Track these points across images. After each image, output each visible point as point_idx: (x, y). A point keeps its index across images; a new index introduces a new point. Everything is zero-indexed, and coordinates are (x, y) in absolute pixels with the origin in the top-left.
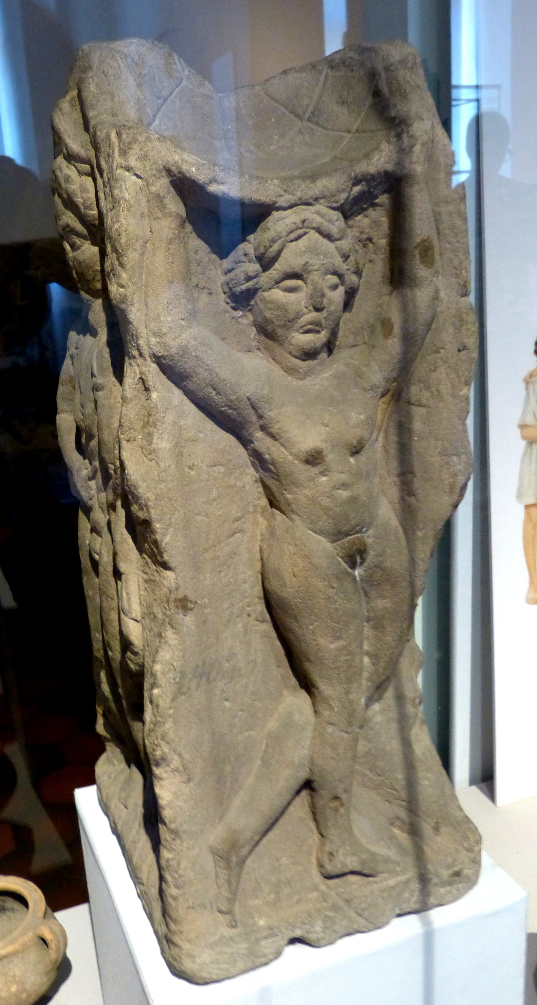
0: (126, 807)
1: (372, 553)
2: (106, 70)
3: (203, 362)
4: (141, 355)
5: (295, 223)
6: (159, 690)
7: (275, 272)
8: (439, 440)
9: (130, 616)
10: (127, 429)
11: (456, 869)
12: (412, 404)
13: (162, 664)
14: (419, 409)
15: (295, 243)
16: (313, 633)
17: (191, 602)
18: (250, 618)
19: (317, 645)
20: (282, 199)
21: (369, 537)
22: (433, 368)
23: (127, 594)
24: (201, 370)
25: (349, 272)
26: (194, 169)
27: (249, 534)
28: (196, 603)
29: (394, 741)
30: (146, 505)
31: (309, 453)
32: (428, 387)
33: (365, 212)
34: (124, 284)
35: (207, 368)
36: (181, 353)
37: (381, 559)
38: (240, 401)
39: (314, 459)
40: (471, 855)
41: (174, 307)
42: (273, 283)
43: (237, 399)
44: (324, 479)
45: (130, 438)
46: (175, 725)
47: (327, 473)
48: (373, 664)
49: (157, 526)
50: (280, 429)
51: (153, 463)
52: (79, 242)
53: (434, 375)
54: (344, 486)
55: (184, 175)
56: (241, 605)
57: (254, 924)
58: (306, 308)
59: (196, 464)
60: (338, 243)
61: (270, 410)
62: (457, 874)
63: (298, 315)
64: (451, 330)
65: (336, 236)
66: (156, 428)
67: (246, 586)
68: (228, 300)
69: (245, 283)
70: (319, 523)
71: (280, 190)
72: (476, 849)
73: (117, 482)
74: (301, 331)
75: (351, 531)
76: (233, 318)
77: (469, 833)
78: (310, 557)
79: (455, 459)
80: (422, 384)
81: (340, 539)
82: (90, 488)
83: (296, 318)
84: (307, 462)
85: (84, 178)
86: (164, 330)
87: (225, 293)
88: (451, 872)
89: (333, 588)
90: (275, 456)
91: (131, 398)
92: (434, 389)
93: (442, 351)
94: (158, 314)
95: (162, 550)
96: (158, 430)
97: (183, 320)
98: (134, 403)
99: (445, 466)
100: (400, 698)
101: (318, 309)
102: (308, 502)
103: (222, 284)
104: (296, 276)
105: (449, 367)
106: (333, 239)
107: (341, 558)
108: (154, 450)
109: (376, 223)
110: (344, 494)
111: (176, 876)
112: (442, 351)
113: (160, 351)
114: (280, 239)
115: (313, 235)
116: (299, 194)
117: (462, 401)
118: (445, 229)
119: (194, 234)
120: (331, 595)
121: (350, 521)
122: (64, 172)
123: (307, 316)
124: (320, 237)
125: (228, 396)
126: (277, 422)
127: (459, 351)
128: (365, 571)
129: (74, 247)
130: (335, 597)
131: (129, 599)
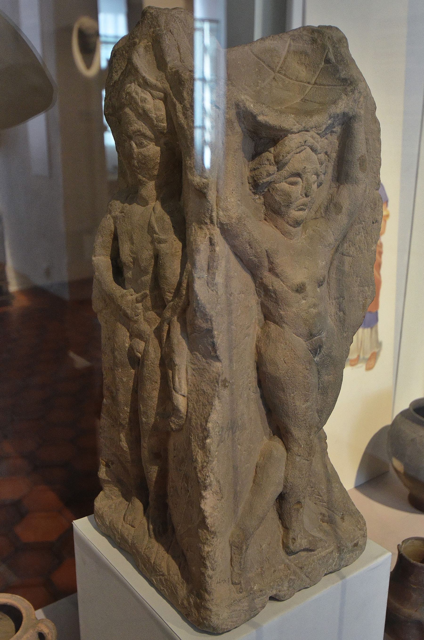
0: (133, 526)
2: (172, 30)
4: (212, 222)
5: (300, 142)
6: (210, 439)
7: (285, 172)
9: (180, 393)
11: (355, 542)
14: (348, 257)
15: (298, 155)
16: (293, 398)
18: (249, 391)
20: (296, 127)
23: (179, 378)
26: (252, 105)
30: (210, 320)
34: (207, 176)
39: (300, 289)
40: (361, 532)
44: (304, 301)
46: (218, 462)
49: (216, 333)
50: (282, 270)
52: (146, 143)
53: (358, 237)
54: (315, 306)
55: (246, 109)
57: (252, 589)
58: (301, 195)
62: (356, 545)
64: (369, 210)
68: (251, 188)
71: (294, 121)
72: (365, 528)
73: (180, 304)
77: (360, 520)
82: (137, 308)
84: (297, 291)
85: (157, 101)
86: (230, 207)
87: (249, 183)
88: (353, 544)
89: (307, 369)
90: (276, 287)
94: (226, 197)
95: (217, 349)
101: (307, 196)
103: (248, 177)
104: (298, 175)
105: (367, 233)
108: (216, 284)
110: (313, 311)
111: (213, 562)
113: (225, 220)
116: (304, 125)
122: (140, 95)
127: (373, 223)
129: (140, 145)
130: (308, 375)
131: (180, 382)
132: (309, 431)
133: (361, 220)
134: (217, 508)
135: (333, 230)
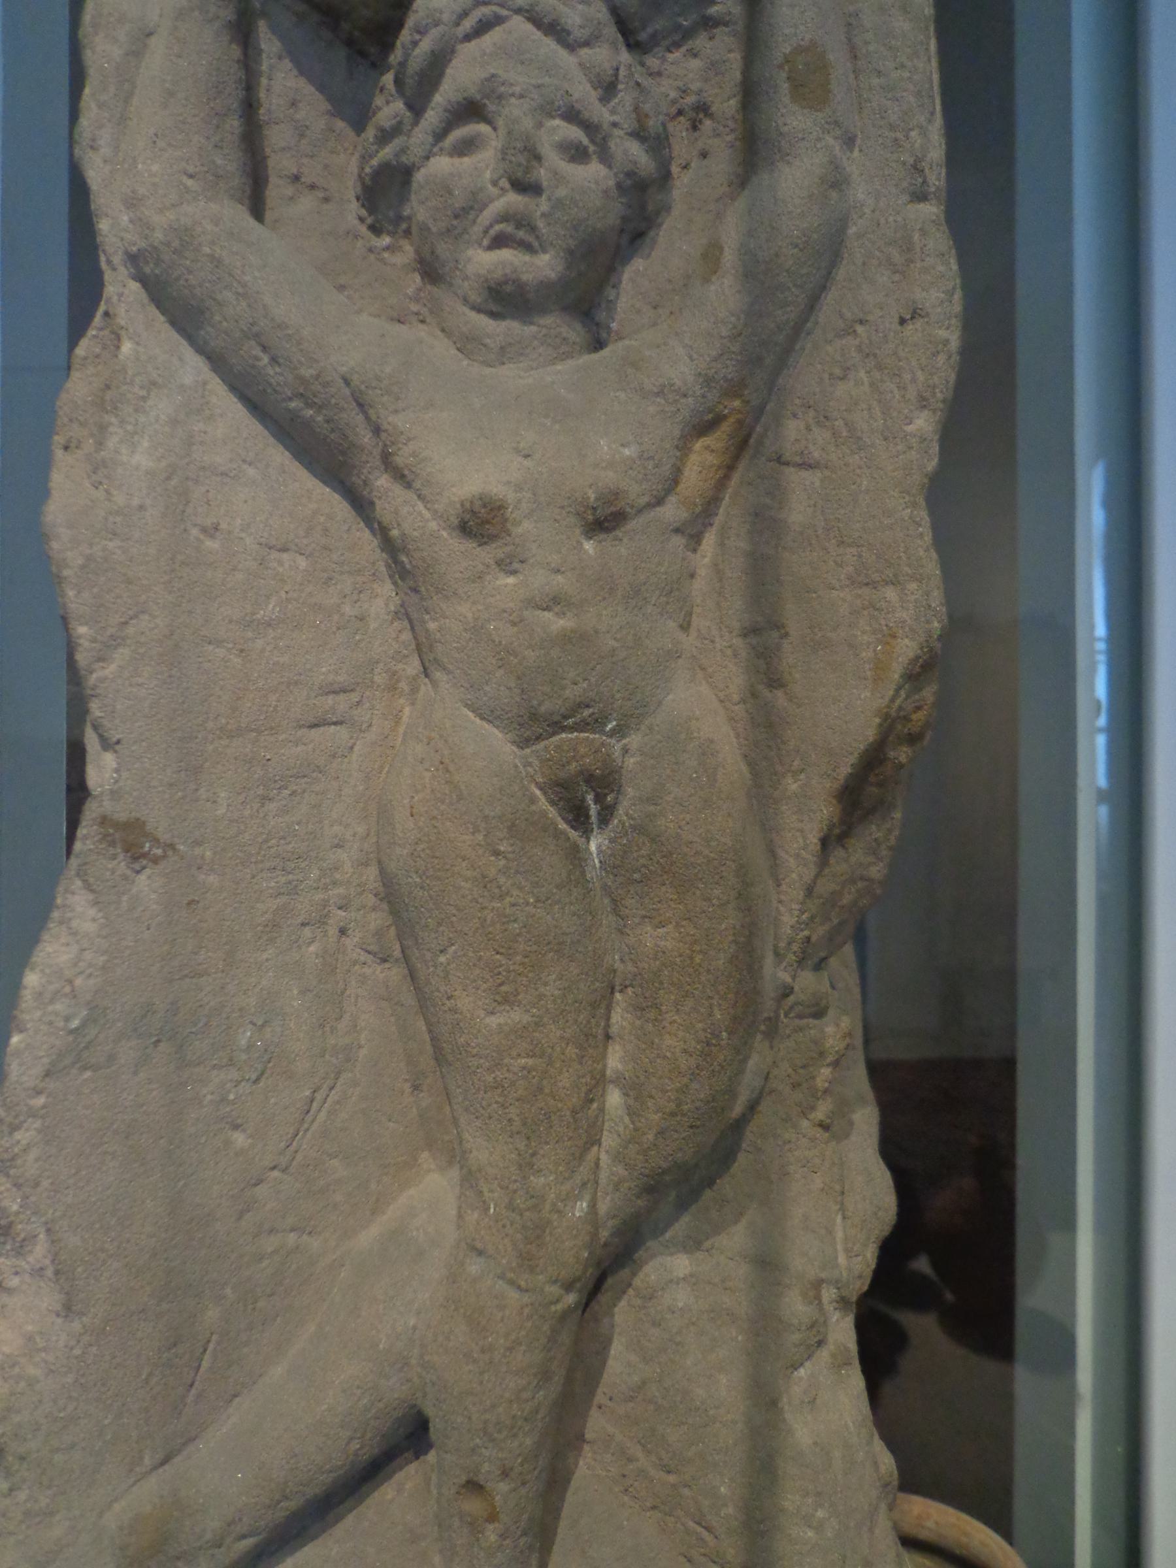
1: (630, 791)
3: (230, 275)
8: (850, 546)
10: (66, 420)
12: (787, 464)
13: (42, 971)
14: (804, 474)
17: (156, 841)
19: (454, 1010)
21: (630, 753)
22: (837, 371)
24: (228, 295)
25: (621, 133)
27: (371, 736)
28: (172, 846)
29: (723, 1379)
31: (468, 505)
32: (824, 419)
33: (690, 44)
35: (240, 290)
36: (176, 244)
37: (652, 808)
38: (326, 385)
39: (481, 522)
41: (170, 145)
42: (431, 139)
43: (318, 376)
45: (69, 441)
47: (516, 566)
48: (632, 1113)
50: (414, 454)
51: (100, 494)
54: (555, 602)
56: (319, 896)
58: (495, 183)
59: (223, 526)
60: (585, 52)
61: (396, 411)
63: (474, 205)
65: (578, 34)
66: (117, 416)
67: (342, 855)
68: (364, 213)
69: (377, 152)
70: (487, 688)
74: (486, 242)
75: (565, 717)
76: (370, 250)
78: (452, 768)
79: (891, 593)
80: (812, 413)
81: (539, 738)
83: (472, 208)
86: (142, 191)
89: (497, 853)
91: (85, 358)
92: (839, 423)
93: (860, 329)
96: (122, 422)
97: (191, 176)
98: (91, 370)
99: (866, 613)
100: (767, 1265)
101: (522, 186)
102: (467, 635)
105: (880, 367)
106: (571, 39)
107: (541, 789)
109: (714, 67)
110: (558, 623)
112: (860, 329)
114: (436, 25)
115: (519, 26)
117: (911, 448)
118: (867, 43)
119: (287, 64)
120: (492, 872)
121: (563, 688)
123: (496, 203)
124: (538, 34)
125: (296, 368)
126: (409, 439)
127: (902, 321)
128: (611, 841)
130: (502, 880)
132: (522, 1146)
133: (848, 315)
134: (44, 1349)
135: (686, 341)
